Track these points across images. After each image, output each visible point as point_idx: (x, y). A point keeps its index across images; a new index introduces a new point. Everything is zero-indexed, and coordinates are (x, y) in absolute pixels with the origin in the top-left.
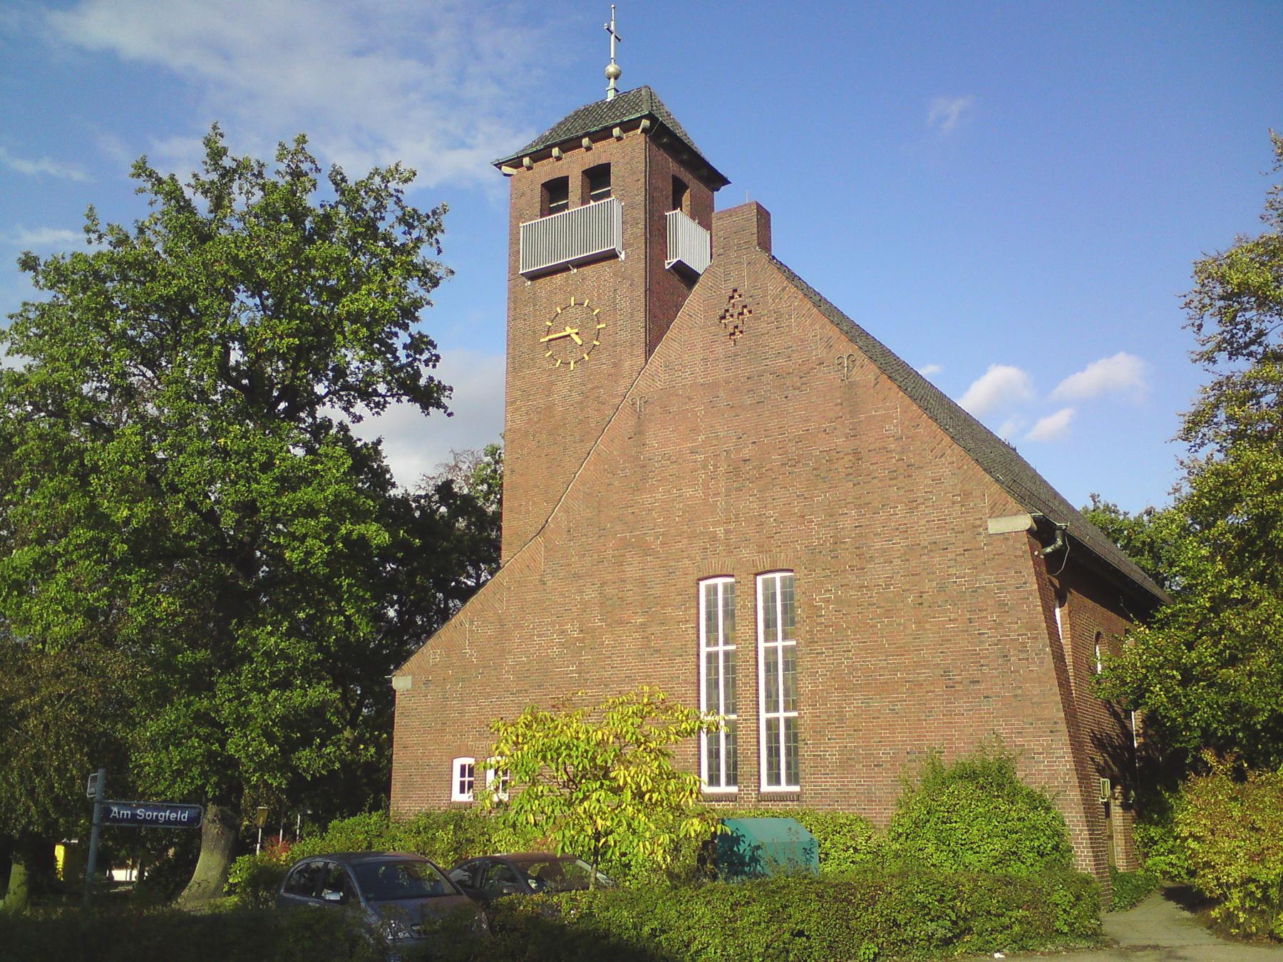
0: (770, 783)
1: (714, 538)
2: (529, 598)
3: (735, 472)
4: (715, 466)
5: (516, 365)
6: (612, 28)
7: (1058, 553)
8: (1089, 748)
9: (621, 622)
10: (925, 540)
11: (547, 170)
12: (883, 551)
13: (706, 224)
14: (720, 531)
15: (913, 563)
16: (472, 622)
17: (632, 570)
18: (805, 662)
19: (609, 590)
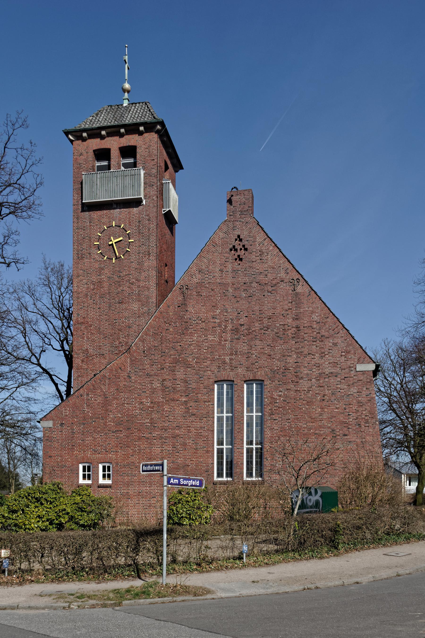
1: (224, 363)
2: (121, 385)
9: (173, 400)
10: (327, 371)
11: (95, 144)
12: (307, 374)
16: (88, 395)
17: (180, 374)
18: (268, 424)
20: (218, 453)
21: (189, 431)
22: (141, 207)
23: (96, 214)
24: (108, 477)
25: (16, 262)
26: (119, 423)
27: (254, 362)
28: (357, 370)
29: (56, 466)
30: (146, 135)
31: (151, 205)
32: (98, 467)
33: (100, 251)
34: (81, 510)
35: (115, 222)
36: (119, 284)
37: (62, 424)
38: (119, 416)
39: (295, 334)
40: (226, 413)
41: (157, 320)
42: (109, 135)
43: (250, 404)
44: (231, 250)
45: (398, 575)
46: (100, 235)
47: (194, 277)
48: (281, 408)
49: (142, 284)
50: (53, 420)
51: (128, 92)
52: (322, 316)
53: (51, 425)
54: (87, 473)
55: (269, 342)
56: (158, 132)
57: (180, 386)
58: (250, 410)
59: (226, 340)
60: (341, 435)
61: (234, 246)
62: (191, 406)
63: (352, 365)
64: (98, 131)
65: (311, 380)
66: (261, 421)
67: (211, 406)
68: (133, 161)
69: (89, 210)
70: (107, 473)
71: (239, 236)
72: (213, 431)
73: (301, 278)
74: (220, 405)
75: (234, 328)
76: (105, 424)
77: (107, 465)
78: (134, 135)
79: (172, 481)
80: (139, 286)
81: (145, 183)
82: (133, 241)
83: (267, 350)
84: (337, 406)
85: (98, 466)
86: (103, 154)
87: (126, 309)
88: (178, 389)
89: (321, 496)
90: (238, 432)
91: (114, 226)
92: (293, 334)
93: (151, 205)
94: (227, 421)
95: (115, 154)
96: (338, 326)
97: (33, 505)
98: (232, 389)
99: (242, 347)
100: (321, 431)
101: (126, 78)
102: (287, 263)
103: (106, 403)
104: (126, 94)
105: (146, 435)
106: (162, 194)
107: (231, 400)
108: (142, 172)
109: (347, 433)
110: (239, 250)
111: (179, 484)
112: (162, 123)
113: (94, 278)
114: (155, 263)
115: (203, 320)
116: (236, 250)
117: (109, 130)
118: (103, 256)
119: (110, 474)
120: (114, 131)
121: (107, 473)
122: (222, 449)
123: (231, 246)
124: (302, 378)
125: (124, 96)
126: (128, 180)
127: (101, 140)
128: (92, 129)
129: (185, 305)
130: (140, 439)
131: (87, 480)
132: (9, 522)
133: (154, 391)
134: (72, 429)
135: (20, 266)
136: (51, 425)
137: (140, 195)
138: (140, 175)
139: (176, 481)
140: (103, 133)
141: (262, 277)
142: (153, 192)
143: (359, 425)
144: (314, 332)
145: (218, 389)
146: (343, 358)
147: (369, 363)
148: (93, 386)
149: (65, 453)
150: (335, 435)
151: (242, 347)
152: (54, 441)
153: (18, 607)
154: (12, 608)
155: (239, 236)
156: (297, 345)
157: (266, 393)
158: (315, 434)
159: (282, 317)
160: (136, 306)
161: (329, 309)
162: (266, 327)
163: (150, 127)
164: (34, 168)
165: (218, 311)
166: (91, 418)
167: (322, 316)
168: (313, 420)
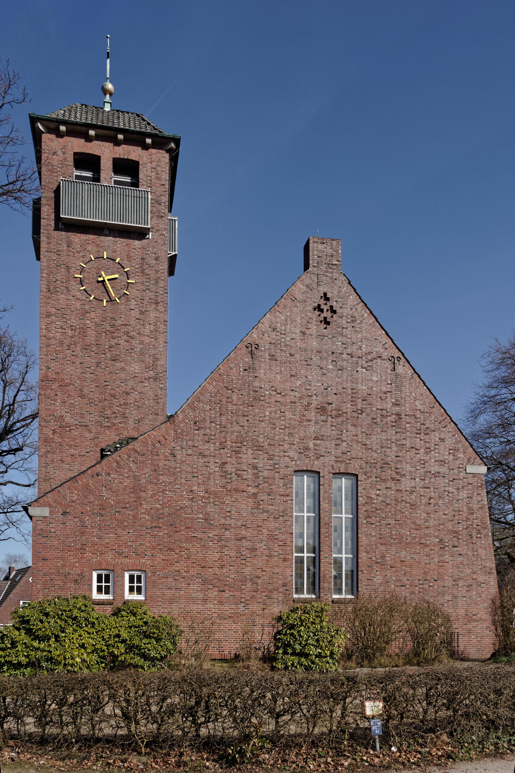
2: (160, 464)
9: (237, 490)
11: (78, 145)
22: (145, 241)
23: (77, 238)
24: (137, 591)
27: (345, 451)
28: (467, 472)
29: (53, 573)
32: (124, 577)
33: (84, 288)
35: (107, 253)
36: (111, 334)
37: (65, 513)
38: (156, 507)
39: (395, 423)
40: (307, 513)
41: (214, 383)
44: (315, 309)
46: (84, 266)
47: (266, 335)
48: (380, 510)
50: (50, 506)
52: (427, 405)
54: (104, 584)
56: (169, 151)
57: (249, 475)
60: (450, 547)
61: (319, 305)
62: (262, 501)
63: (461, 466)
64: (84, 129)
65: (415, 479)
67: (289, 502)
68: (129, 181)
70: (135, 585)
71: (325, 294)
73: (401, 357)
75: (319, 407)
77: (136, 574)
78: (136, 148)
82: (134, 282)
83: (361, 438)
84: (446, 512)
85: (124, 575)
86: (87, 162)
87: (123, 369)
88: (245, 477)
90: (326, 537)
91: (105, 257)
92: (393, 422)
94: (308, 522)
96: (446, 418)
100: (427, 540)
101: (108, 76)
103: (137, 489)
104: (108, 96)
109: (456, 544)
110: (325, 310)
115: (278, 391)
116: (322, 311)
117: (100, 131)
118: (88, 294)
119: (141, 586)
120: (109, 134)
121: (135, 585)
125: (105, 98)
127: (86, 141)
128: (76, 124)
131: (135, 595)
134: (82, 521)
140: (92, 133)
143: (470, 535)
144: (418, 422)
146: (451, 456)
147: (480, 465)
148: (117, 462)
149: (70, 555)
150: (443, 546)
152: (51, 537)
155: (325, 294)
156: (398, 436)
158: (420, 544)
159: (379, 399)
160: (137, 368)
161: (435, 397)
162: (359, 410)
167: (427, 405)
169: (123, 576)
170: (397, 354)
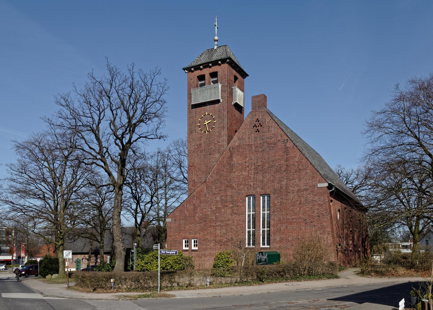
0: (263, 245)
1: (250, 185)
2: (202, 199)
3: (256, 169)
4: (251, 167)
5: (191, 132)
6: (216, 25)
7: (333, 192)
8: (76, 287)
9: (226, 206)
10: (302, 188)
11: (198, 73)
12: (292, 190)
13: (242, 90)
14: (252, 184)
15: (299, 194)
16: (187, 205)
17: (229, 193)
18: (272, 217)
19: (223, 198)
20: (248, 233)
21: (234, 222)
23: (198, 109)
25: (162, 137)
26: (201, 219)
30: (222, 65)
31: (225, 102)
34: (176, 262)
37: (175, 220)
42: (204, 67)
43: (264, 207)
44: (254, 127)
45: (269, 293)
49: (220, 144)
51: (217, 41)
53: (170, 221)
55: (273, 174)
56: (228, 63)
57: (229, 198)
58: (264, 210)
59: (251, 174)
66: (269, 215)
69: (195, 108)
71: (257, 119)
72: (245, 222)
73: (289, 139)
74: (249, 208)
76: (194, 219)
77: (196, 240)
79: (162, 252)
80: (219, 145)
81: (222, 91)
86: (202, 78)
89: (267, 256)
93: (225, 102)
95: (207, 77)
97: (155, 260)
98: (255, 199)
99: (260, 177)
101: (216, 33)
102: (282, 131)
103: (195, 208)
105: (214, 224)
106: (231, 94)
107: (254, 205)
108: (220, 86)
111: (166, 253)
112: (230, 58)
113: (198, 143)
114: (226, 132)
116: (256, 127)
120: (206, 65)
122: (250, 231)
123: (253, 125)
124: (289, 192)
126: (213, 90)
128: (196, 66)
129: (232, 157)
130: (210, 226)
132: (144, 268)
133: (217, 202)
134: (180, 222)
135: (165, 138)
136: (170, 221)
137: (218, 97)
138: (219, 87)
139: (164, 252)
140: (201, 67)
141: (269, 140)
142: (225, 95)
145: (248, 200)
151: (260, 177)
153: (102, 299)
154: (100, 299)
155: (257, 119)
157: (272, 201)
163: (223, 61)
164: (166, 92)
165: (247, 159)
166: (188, 216)
168: (295, 214)
169: (191, 241)
170: (286, 138)
